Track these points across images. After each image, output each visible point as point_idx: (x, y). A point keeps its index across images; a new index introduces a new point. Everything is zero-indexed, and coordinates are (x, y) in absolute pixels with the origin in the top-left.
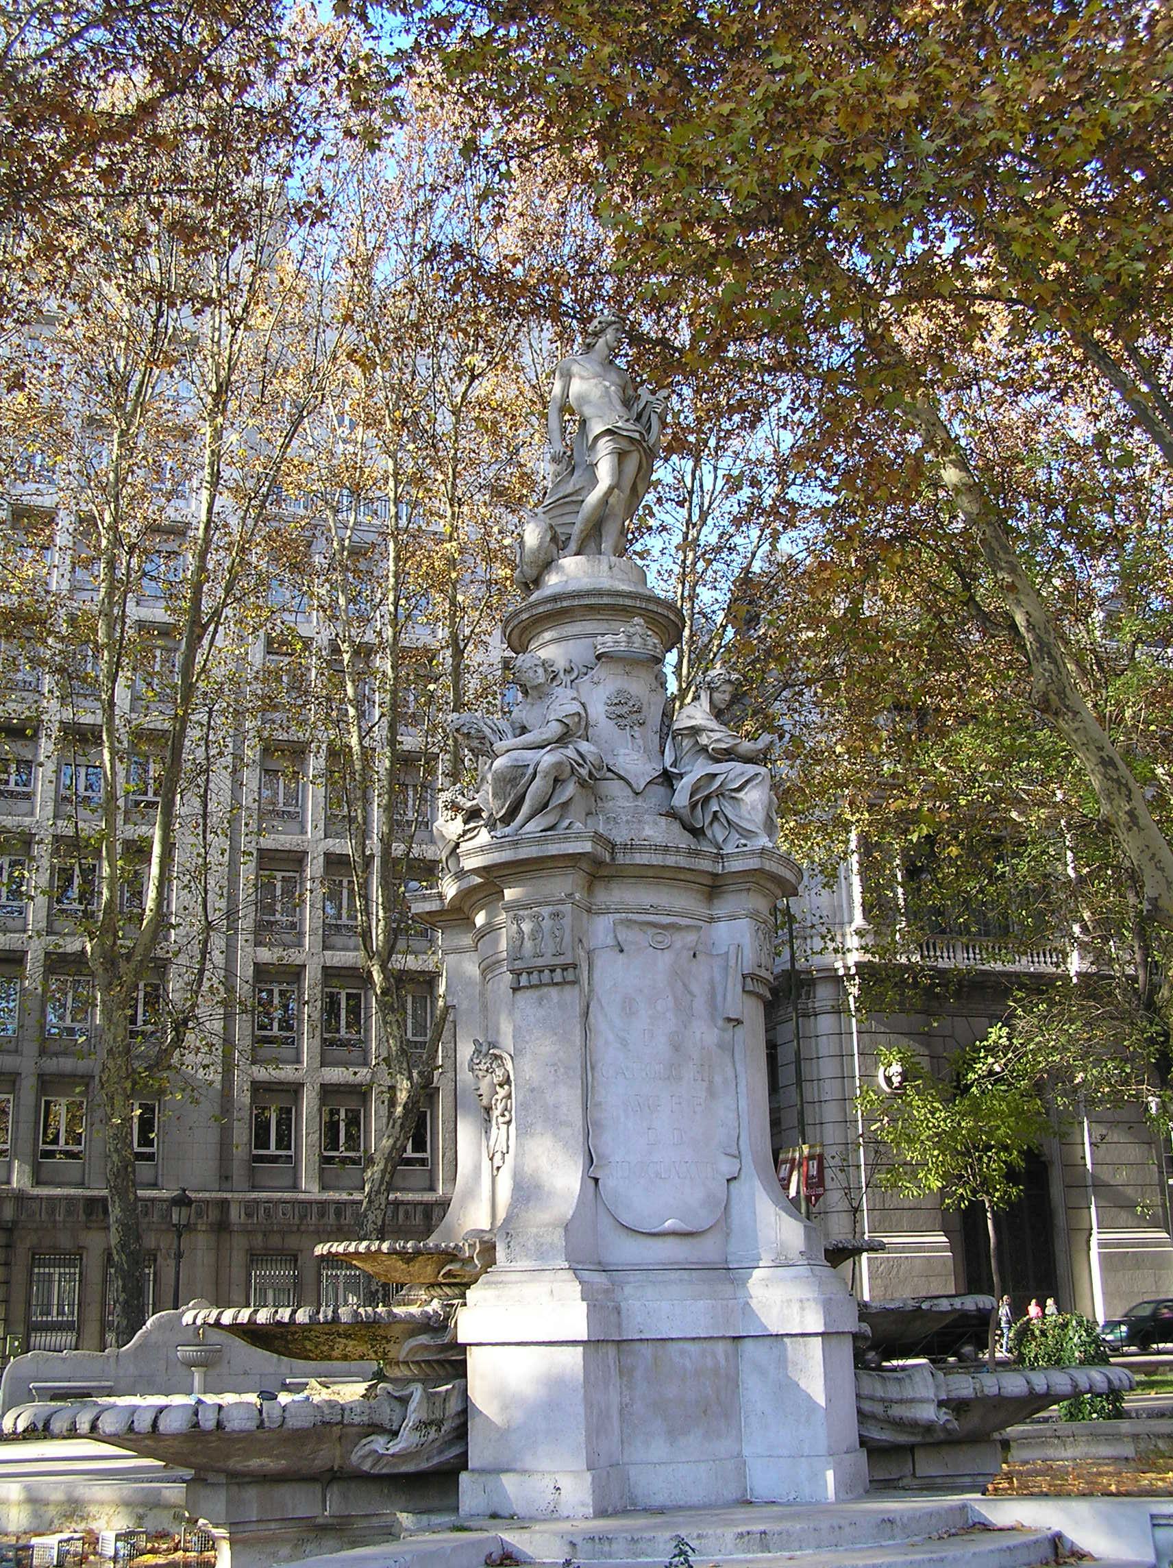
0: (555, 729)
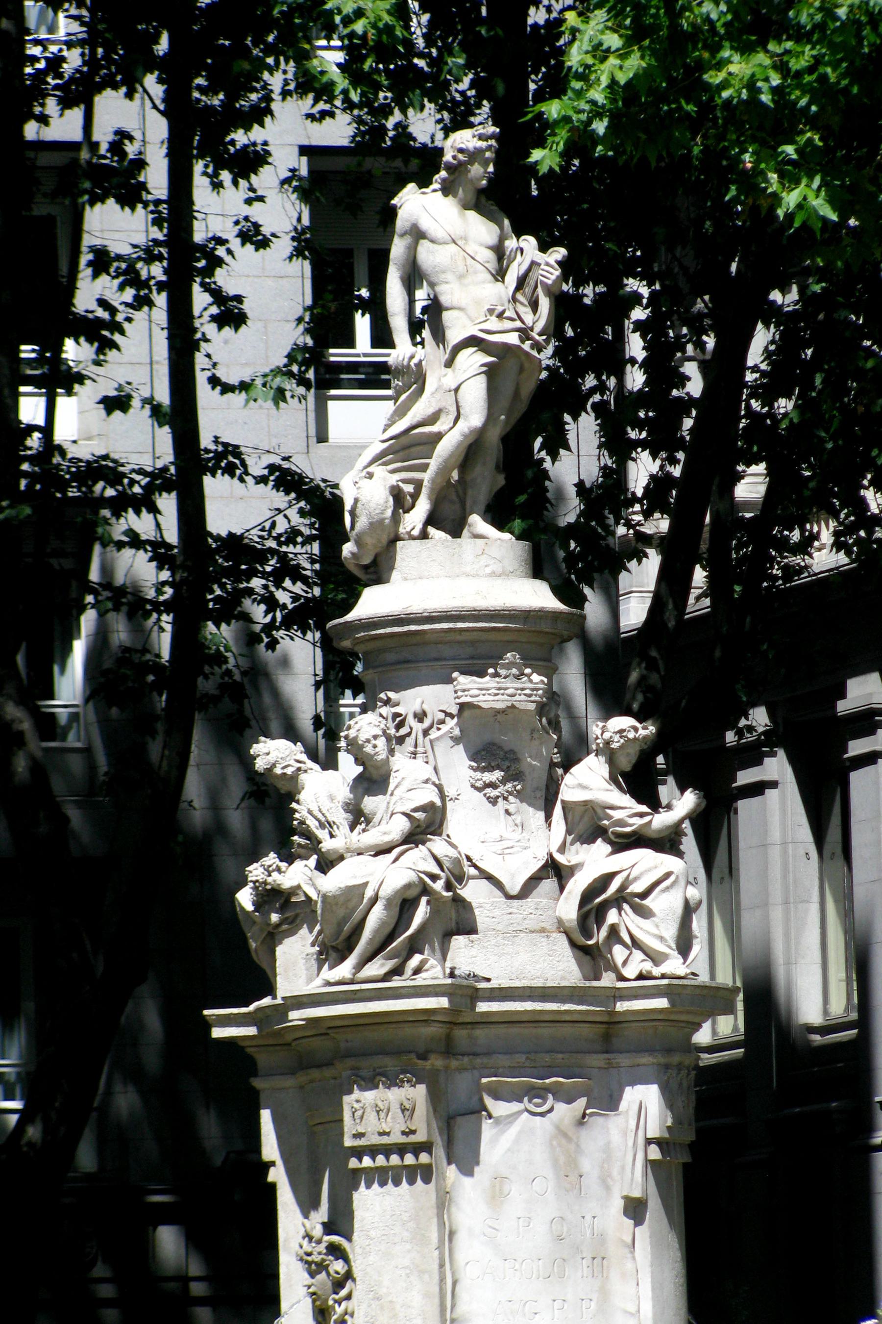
0: (399, 827)
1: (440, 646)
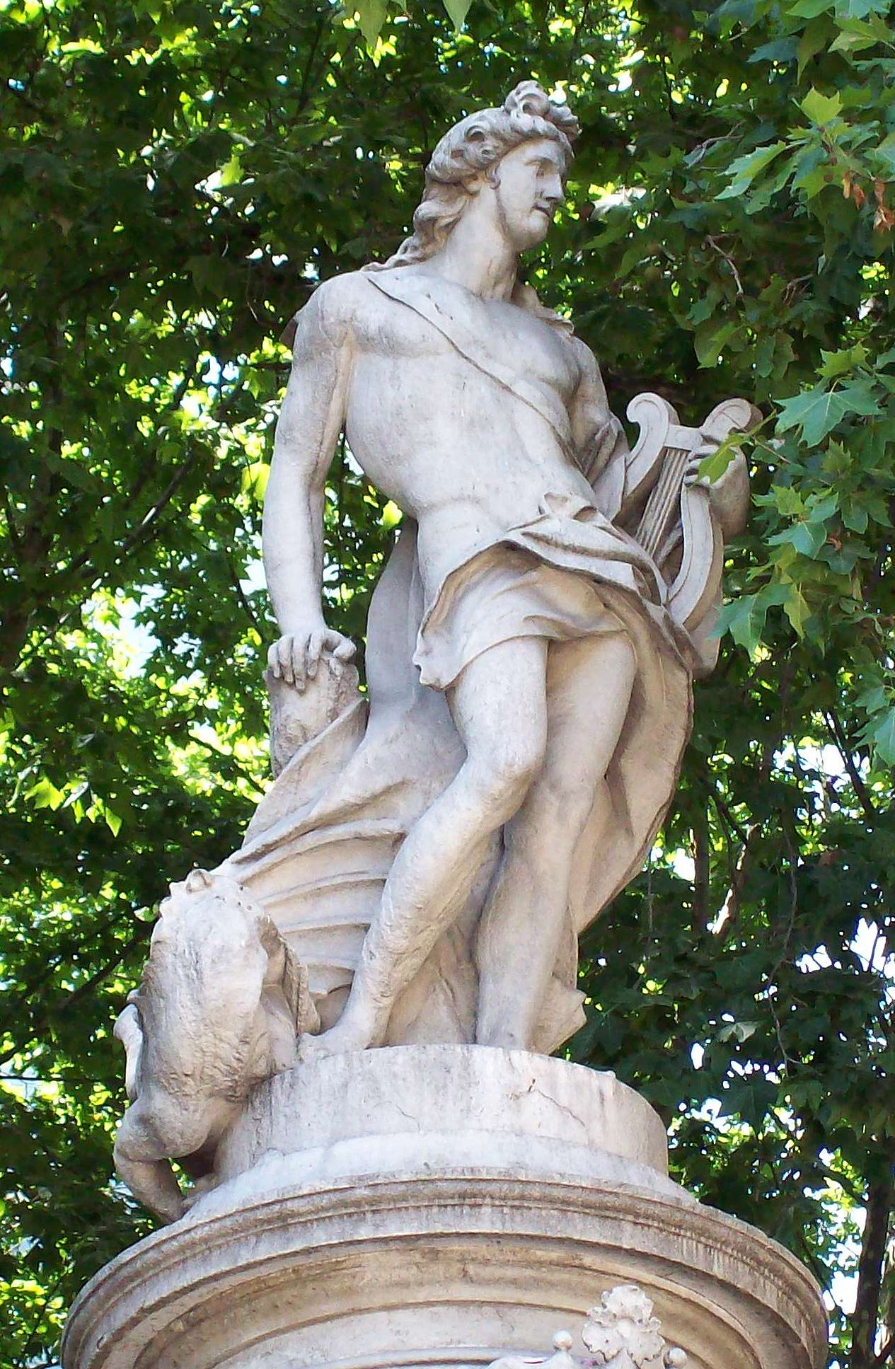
1: (399, 1315)
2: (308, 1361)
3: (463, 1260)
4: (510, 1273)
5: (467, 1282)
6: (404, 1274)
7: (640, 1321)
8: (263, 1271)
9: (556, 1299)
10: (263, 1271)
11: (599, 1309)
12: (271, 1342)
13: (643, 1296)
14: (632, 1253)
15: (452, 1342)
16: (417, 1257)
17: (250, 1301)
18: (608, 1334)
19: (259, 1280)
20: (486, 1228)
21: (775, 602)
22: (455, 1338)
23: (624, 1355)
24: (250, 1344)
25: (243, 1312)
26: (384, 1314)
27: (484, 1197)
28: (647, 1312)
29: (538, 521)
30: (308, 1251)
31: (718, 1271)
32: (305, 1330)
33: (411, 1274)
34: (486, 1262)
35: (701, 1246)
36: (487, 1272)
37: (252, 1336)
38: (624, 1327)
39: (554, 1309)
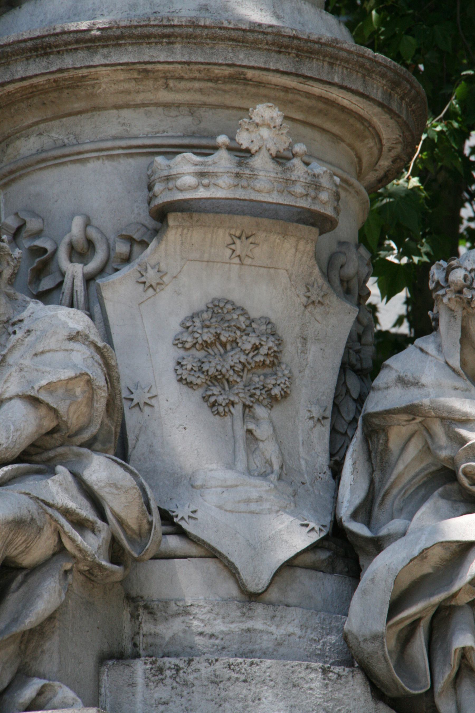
1: (126, 113)
2: (66, 141)
3: (166, 78)
4: (197, 85)
5: (168, 91)
6: (126, 86)
7: (274, 127)
8: (35, 81)
9: (228, 100)
10: (35, 81)
11: (247, 120)
12: (42, 126)
13: (277, 109)
14: (277, 71)
15: (158, 133)
16: (136, 75)
17: (28, 98)
18: (254, 136)
19: (32, 86)
20: (179, 58)
21: (326, 236)
22: (161, 129)
23: (264, 151)
24: (30, 126)
25: (23, 105)
26: (115, 111)
27: (177, 37)
28: (279, 121)
29: (454, 370)
30: (60, 71)
31: (336, 80)
32: (64, 119)
33: (131, 86)
34: (181, 78)
35: (326, 64)
36: (183, 85)
37: (30, 122)
38: (265, 132)
39: (228, 108)
